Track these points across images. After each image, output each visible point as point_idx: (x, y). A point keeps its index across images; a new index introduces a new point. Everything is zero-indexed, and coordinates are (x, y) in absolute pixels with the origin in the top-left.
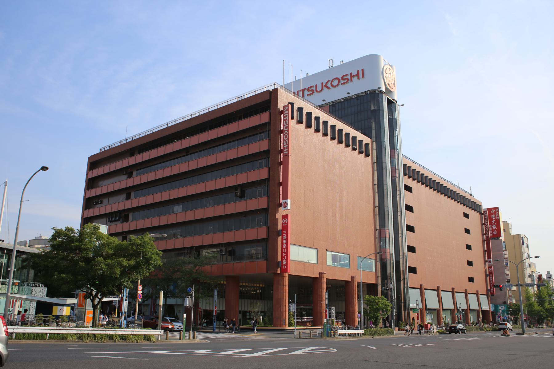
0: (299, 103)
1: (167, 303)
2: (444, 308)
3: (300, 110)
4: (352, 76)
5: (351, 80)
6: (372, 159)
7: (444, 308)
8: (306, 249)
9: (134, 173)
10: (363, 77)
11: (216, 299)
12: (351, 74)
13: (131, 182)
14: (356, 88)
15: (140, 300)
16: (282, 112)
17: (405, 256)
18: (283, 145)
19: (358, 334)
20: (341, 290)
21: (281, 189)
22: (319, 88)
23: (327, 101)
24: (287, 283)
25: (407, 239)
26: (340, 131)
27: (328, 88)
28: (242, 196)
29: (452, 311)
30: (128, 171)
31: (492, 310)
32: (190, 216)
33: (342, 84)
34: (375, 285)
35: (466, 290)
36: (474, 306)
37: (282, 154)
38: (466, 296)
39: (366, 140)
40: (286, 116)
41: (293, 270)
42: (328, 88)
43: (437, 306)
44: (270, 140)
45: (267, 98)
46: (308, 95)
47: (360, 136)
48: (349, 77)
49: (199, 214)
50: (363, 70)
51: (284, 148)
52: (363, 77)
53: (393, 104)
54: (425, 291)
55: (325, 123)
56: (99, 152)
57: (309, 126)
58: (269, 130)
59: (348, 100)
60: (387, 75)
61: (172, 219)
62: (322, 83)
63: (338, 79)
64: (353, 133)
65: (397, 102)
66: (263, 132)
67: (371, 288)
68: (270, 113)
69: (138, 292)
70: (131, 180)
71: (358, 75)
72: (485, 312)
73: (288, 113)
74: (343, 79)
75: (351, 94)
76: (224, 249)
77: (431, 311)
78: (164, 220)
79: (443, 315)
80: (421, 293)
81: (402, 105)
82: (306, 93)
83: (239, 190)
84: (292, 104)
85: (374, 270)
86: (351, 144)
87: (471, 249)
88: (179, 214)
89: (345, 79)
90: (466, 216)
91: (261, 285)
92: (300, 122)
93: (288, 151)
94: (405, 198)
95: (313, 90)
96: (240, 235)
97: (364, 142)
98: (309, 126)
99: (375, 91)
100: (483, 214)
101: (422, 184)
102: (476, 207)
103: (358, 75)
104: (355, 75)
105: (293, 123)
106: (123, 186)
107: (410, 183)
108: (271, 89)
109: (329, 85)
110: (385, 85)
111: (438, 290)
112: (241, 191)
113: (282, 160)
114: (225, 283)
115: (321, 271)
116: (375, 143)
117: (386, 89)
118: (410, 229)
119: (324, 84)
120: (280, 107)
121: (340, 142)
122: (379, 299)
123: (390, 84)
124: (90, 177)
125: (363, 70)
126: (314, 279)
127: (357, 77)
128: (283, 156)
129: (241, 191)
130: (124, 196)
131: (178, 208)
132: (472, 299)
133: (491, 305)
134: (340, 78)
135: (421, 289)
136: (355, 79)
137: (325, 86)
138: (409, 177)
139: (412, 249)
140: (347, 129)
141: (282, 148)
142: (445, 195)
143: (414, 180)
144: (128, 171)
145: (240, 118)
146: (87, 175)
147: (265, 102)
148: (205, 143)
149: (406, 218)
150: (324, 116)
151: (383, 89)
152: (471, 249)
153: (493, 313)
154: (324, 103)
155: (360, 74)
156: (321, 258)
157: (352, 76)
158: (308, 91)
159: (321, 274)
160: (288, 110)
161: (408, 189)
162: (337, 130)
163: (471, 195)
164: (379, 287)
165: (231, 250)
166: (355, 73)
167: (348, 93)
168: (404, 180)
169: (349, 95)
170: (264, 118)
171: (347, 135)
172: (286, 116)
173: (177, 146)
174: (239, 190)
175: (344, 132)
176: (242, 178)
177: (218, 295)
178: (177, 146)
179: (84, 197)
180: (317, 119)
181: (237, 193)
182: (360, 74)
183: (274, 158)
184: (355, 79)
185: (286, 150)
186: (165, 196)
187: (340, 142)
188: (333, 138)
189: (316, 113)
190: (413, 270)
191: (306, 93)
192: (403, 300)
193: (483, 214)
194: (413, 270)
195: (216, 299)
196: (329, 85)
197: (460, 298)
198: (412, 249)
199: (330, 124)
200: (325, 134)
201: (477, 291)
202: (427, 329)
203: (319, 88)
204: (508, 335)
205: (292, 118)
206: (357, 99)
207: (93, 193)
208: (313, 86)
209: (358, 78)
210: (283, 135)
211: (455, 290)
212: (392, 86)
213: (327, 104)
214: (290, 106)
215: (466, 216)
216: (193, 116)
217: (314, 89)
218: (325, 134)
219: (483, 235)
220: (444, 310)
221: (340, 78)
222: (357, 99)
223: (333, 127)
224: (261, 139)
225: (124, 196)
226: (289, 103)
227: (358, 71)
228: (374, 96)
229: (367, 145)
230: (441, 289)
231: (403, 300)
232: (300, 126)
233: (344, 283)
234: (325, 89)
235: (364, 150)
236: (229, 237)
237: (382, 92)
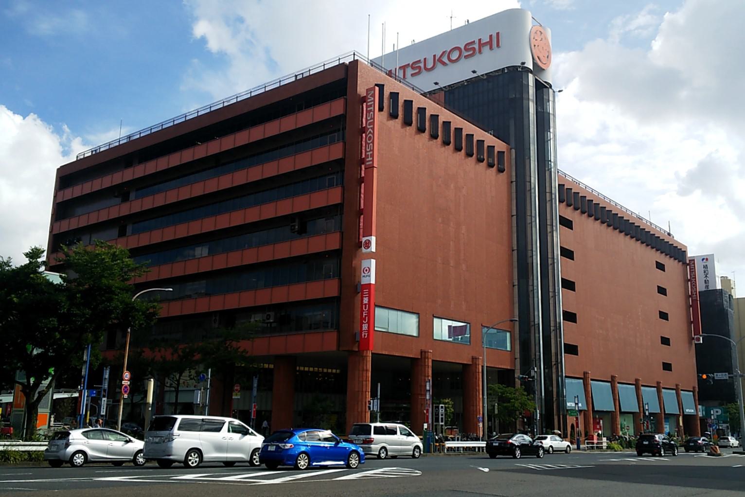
0: (391, 86)
1: (179, 401)
2: (623, 410)
3: (394, 96)
4: (481, 45)
5: (480, 52)
6: (510, 176)
7: (623, 410)
8: (399, 313)
9: (132, 196)
10: (498, 45)
11: (255, 393)
12: (480, 40)
13: (125, 209)
14: (487, 63)
15: (126, 396)
16: (364, 100)
17: (558, 328)
18: (366, 152)
19: (479, 448)
20: (454, 379)
21: (362, 220)
22: (430, 65)
23: (442, 85)
24: (369, 366)
25: (563, 300)
26: (459, 131)
27: (444, 64)
28: (303, 231)
29: (584, 413)
30: (122, 192)
31: (700, 414)
32: (221, 262)
33: (466, 57)
34: (511, 372)
35: (658, 383)
36: (671, 408)
37: (363, 166)
38: (659, 392)
39: (500, 146)
40: (371, 106)
41: (378, 347)
42: (444, 64)
43: (610, 407)
44: (345, 144)
45: (341, 75)
46: (412, 75)
47: (489, 139)
48: (476, 46)
49: (235, 259)
50: (498, 34)
51: (367, 156)
52: (498, 45)
53: (545, 90)
54: (642, 388)
55: (434, 118)
56: (75, 160)
57: (407, 122)
58: (344, 129)
59: (474, 83)
60: (537, 43)
61: (191, 268)
62: (435, 56)
63: (458, 48)
64: (479, 134)
65: (551, 87)
66: (335, 131)
67: (503, 376)
68: (346, 99)
69: (123, 382)
70: (127, 204)
71: (490, 43)
72: (688, 419)
73: (374, 101)
74: (466, 49)
75: (479, 73)
76: (272, 314)
77: (668, 416)
78: (177, 269)
79: (620, 420)
80: (586, 385)
81: (560, 91)
82: (409, 71)
83: (297, 221)
84: (381, 87)
85: (509, 349)
86: (475, 152)
87: (667, 319)
88: (202, 259)
89: (471, 50)
90: (660, 266)
91: (334, 371)
92: (393, 116)
93: (373, 161)
94: (559, 237)
95: (420, 67)
96: (297, 292)
97: (496, 150)
98: (407, 122)
99: (515, 67)
100: (688, 264)
101: (590, 216)
102: (677, 253)
103: (490, 43)
104: (486, 44)
105: (380, 118)
106: (114, 213)
107: (569, 213)
108: (347, 61)
109: (445, 59)
110: (533, 59)
111: (612, 381)
112: (302, 223)
113: (363, 175)
114: (272, 366)
115: (423, 348)
116: (513, 151)
117: (534, 64)
118: (569, 285)
119: (437, 58)
120: (361, 90)
121: (458, 149)
122: (505, 397)
123: (541, 57)
124: (60, 200)
125: (498, 34)
126: (413, 360)
127: (488, 47)
128: (365, 169)
129: (302, 223)
130: (115, 232)
131: (202, 251)
132: (669, 396)
133: (700, 407)
134: (463, 48)
135: (585, 378)
136: (486, 49)
137: (439, 61)
138: (569, 205)
139: (570, 317)
140: (469, 128)
141: (364, 156)
142: (626, 235)
143: (576, 209)
144: (122, 192)
145: (300, 109)
146: (55, 197)
147: (339, 82)
148: (553, 220)
149: (561, 268)
150: (432, 108)
151: (530, 65)
152: (667, 319)
153: (702, 419)
154: (437, 87)
155: (493, 42)
156: (425, 328)
157: (481, 45)
158: (413, 68)
159: (423, 353)
160: (373, 96)
161: (566, 223)
162: (452, 129)
163: (669, 234)
164: (518, 374)
165: (286, 317)
166: (486, 39)
167: (474, 72)
168: (559, 209)
169: (475, 75)
170: (336, 108)
171: (470, 137)
172: (371, 106)
173: (200, 151)
174: (297, 221)
175: (464, 133)
176: (301, 203)
177: (258, 386)
178: (200, 151)
179: (50, 232)
180: (422, 111)
181: (294, 226)
182: (493, 42)
183: (348, 172)
184: (486, 49)
185: (370, 159)
186: (181, 231)
187: (458, 149)
188: (446, 143)
189: (419, 101)
190: (572, 349)
191: (409, 71)
192: (555, 396)
193: (688, 264)
194: (572, 349)
195: (255, 393)
196: (445, 59)
197: (649, 394)
198: (570, 317)
199: (441, 120)
200: (434, 136)
201: (677, 385)
202: (593, 443)
203: (430, 65)
204: (719, 455)
205: (381, 109)
206: (488, 82)
207: (65, 226)
208: (419, 61)
209: (491, 48)
210: (366, 136)
211: (641, 383)
212: (544, 60)
213: (441, 89)
214: (377, 88)
215: (660, 266)
216: (226, 104)
217: (422, 65)
218: (434, 136)
219: (688, 297)
220: (622, 413)
221: (463, 48)
222: (488, 82)
223: (447, 124)
224: (332, 142)
225: (115, 232)
226: (376, 85)
227: (491, 36)
228: (514, 75)
229: (501, 153)
230: (617, 380)
231: (555, 396)
232: (392, 123)
233: (461, 366)
234: (439, 65)
235: (495, 161)
236: (281, 294)
237: (528, 70)
